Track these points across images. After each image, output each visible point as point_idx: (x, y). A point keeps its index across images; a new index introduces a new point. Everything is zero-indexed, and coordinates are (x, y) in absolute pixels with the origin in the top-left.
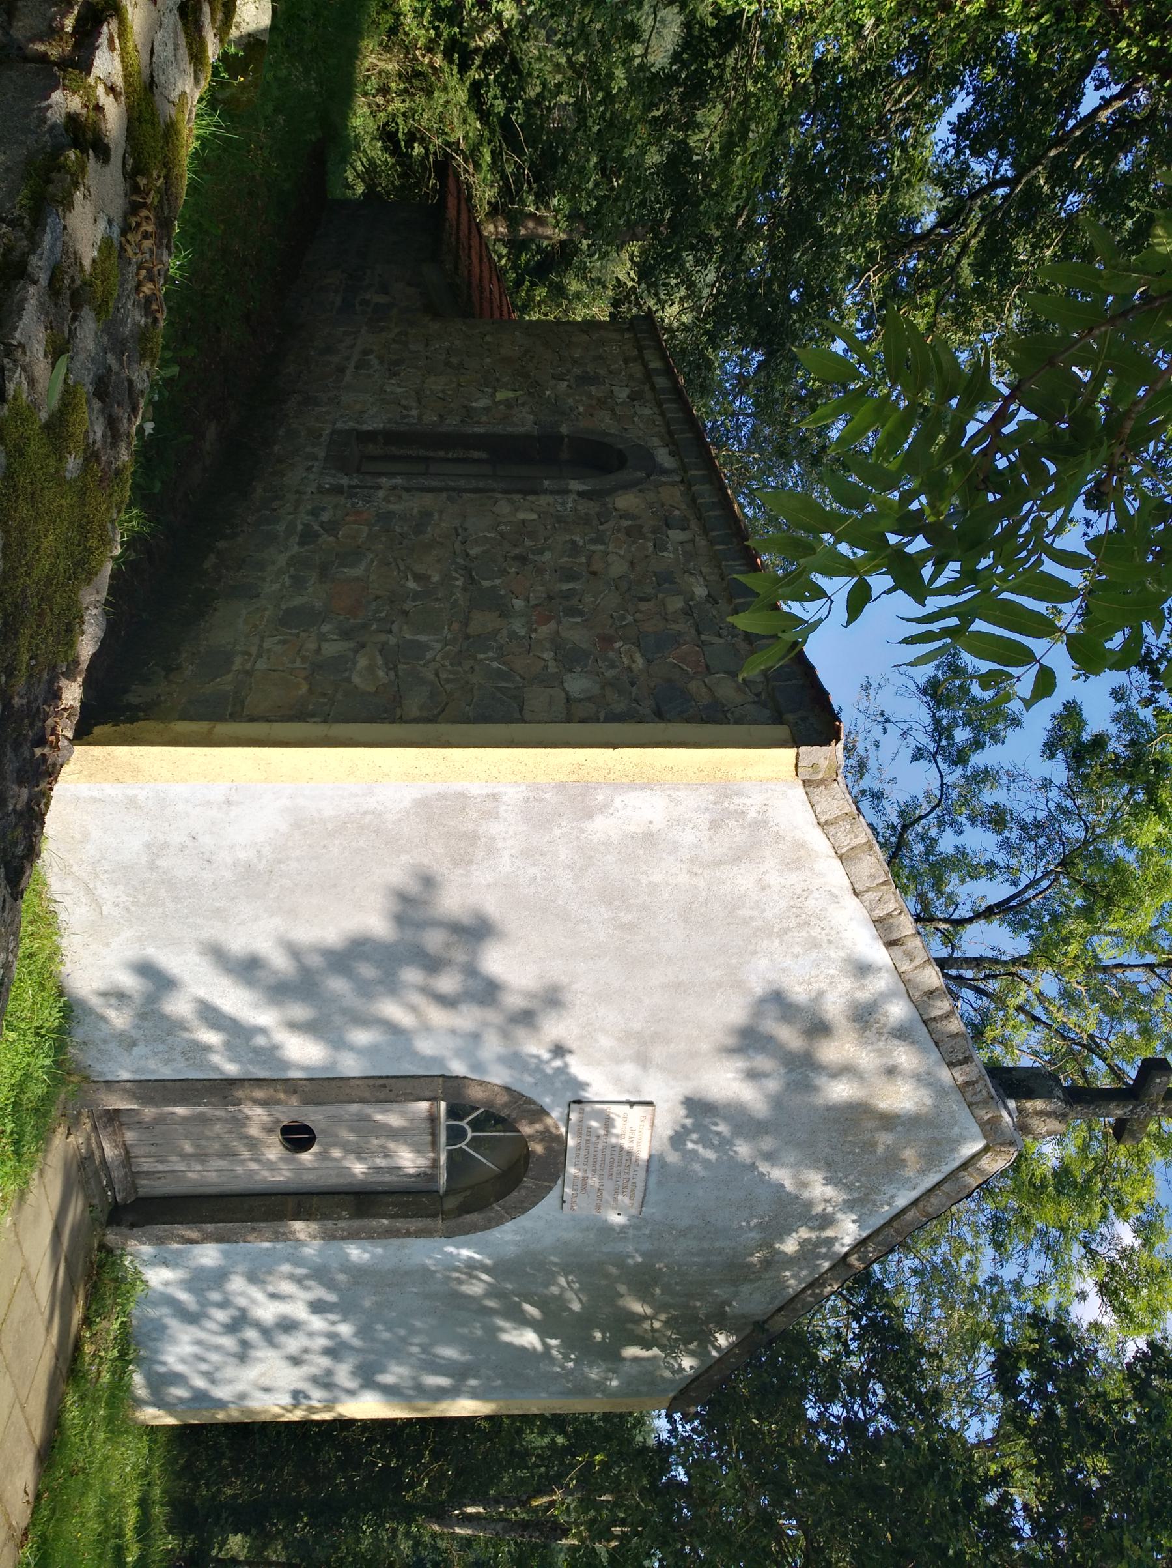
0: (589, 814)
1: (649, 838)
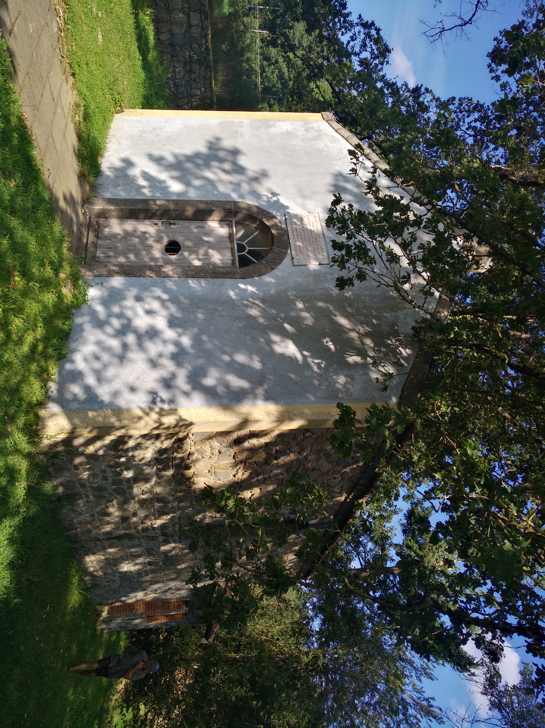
0: (270, 127)
1: (289, 133)
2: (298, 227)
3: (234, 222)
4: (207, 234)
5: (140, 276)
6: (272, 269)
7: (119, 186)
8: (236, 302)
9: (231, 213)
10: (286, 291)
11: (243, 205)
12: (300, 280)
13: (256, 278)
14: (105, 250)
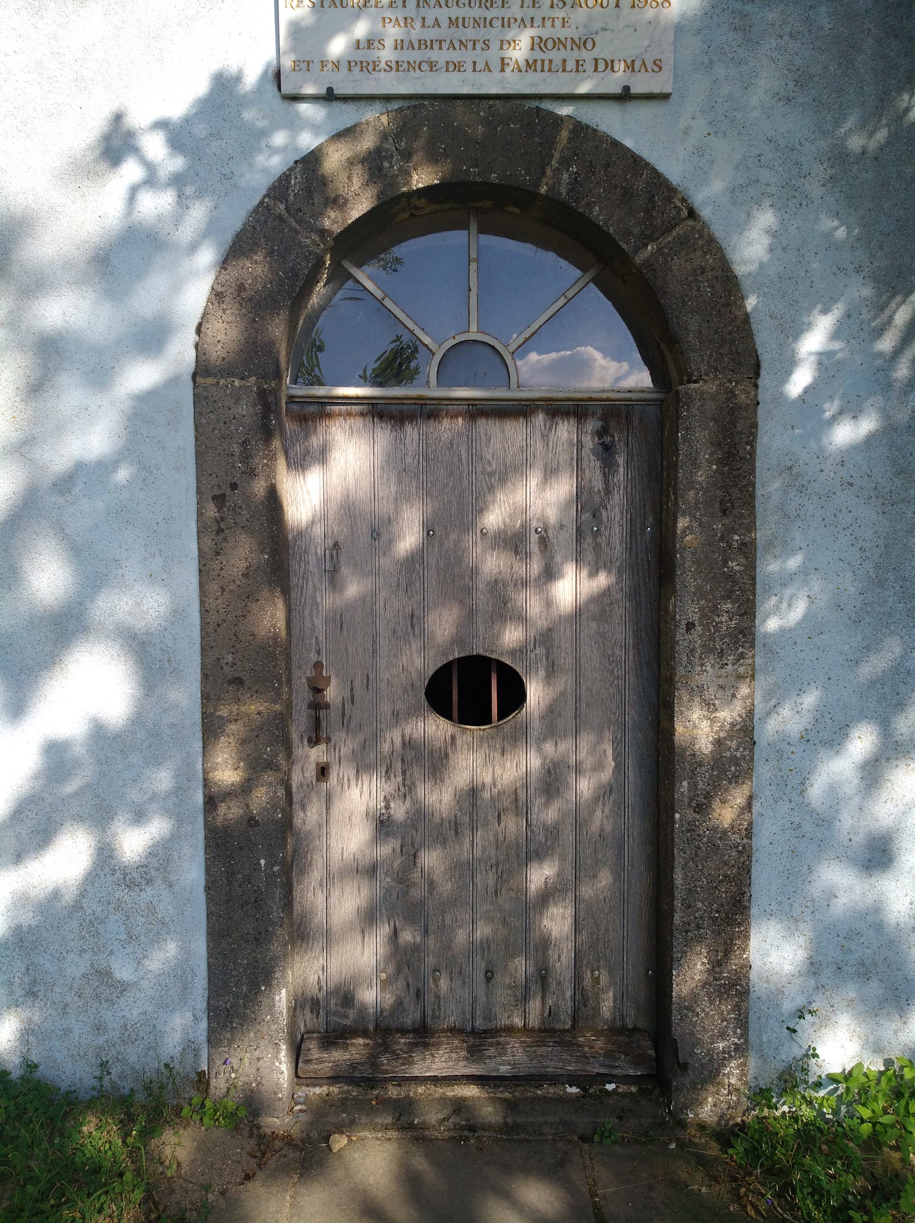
2: (393, 33)
3: (300, 391)
4: (379, 533)
5: (746, 852)
6: (692, 214)
7: (105, 975)
8: (902, 417)
9: (250, 406)
10: (840, 157)
11: (225, 333)
12: (767, 81)
13: (751, 303)
14: (501, 996)
